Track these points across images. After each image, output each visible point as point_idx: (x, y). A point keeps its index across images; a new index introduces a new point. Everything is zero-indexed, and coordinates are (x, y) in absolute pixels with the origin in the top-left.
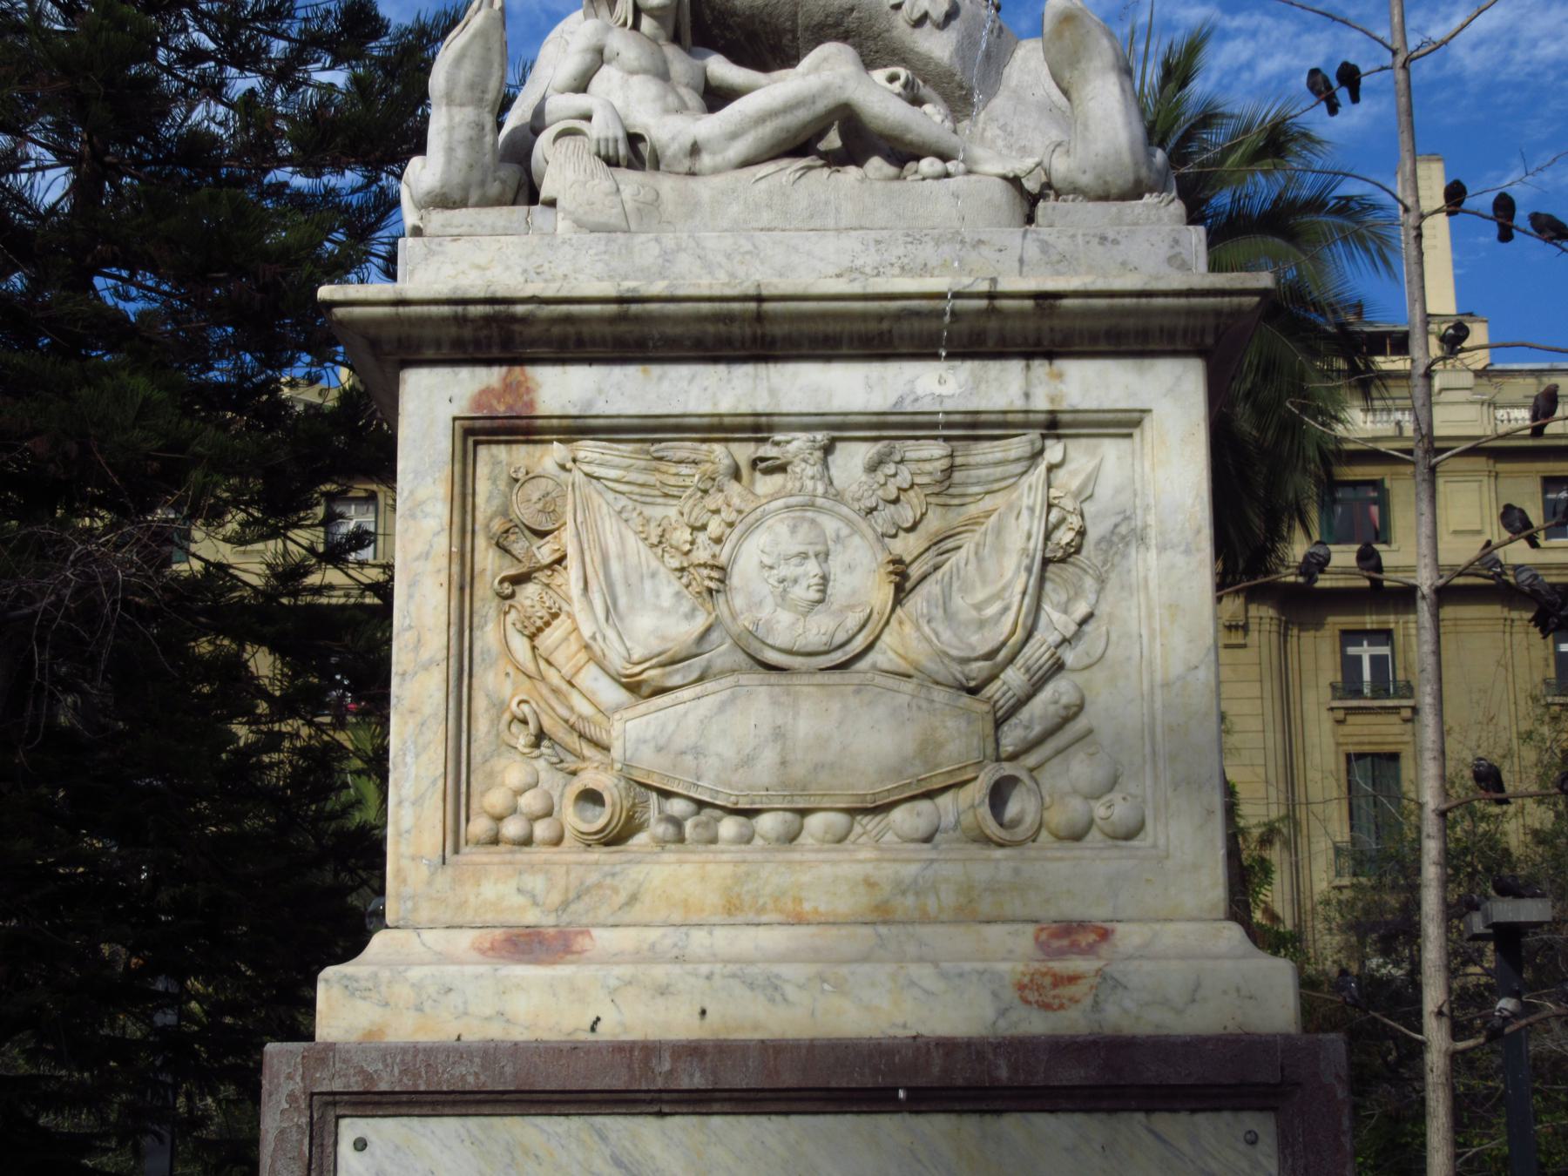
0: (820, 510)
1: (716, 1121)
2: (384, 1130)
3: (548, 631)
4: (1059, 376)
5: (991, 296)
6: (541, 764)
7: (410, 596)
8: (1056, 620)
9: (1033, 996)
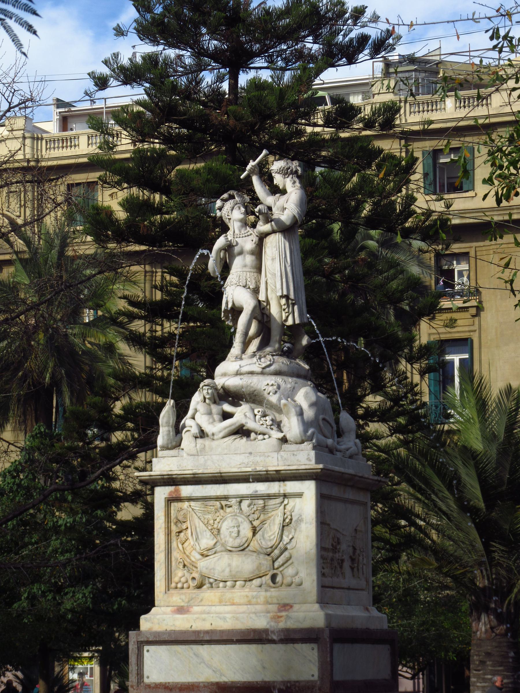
0: (238, 516)
1: (213, 646)
4: (285, 485)
5: (267, 471)
6: (185, 571)
8: (286, 539)
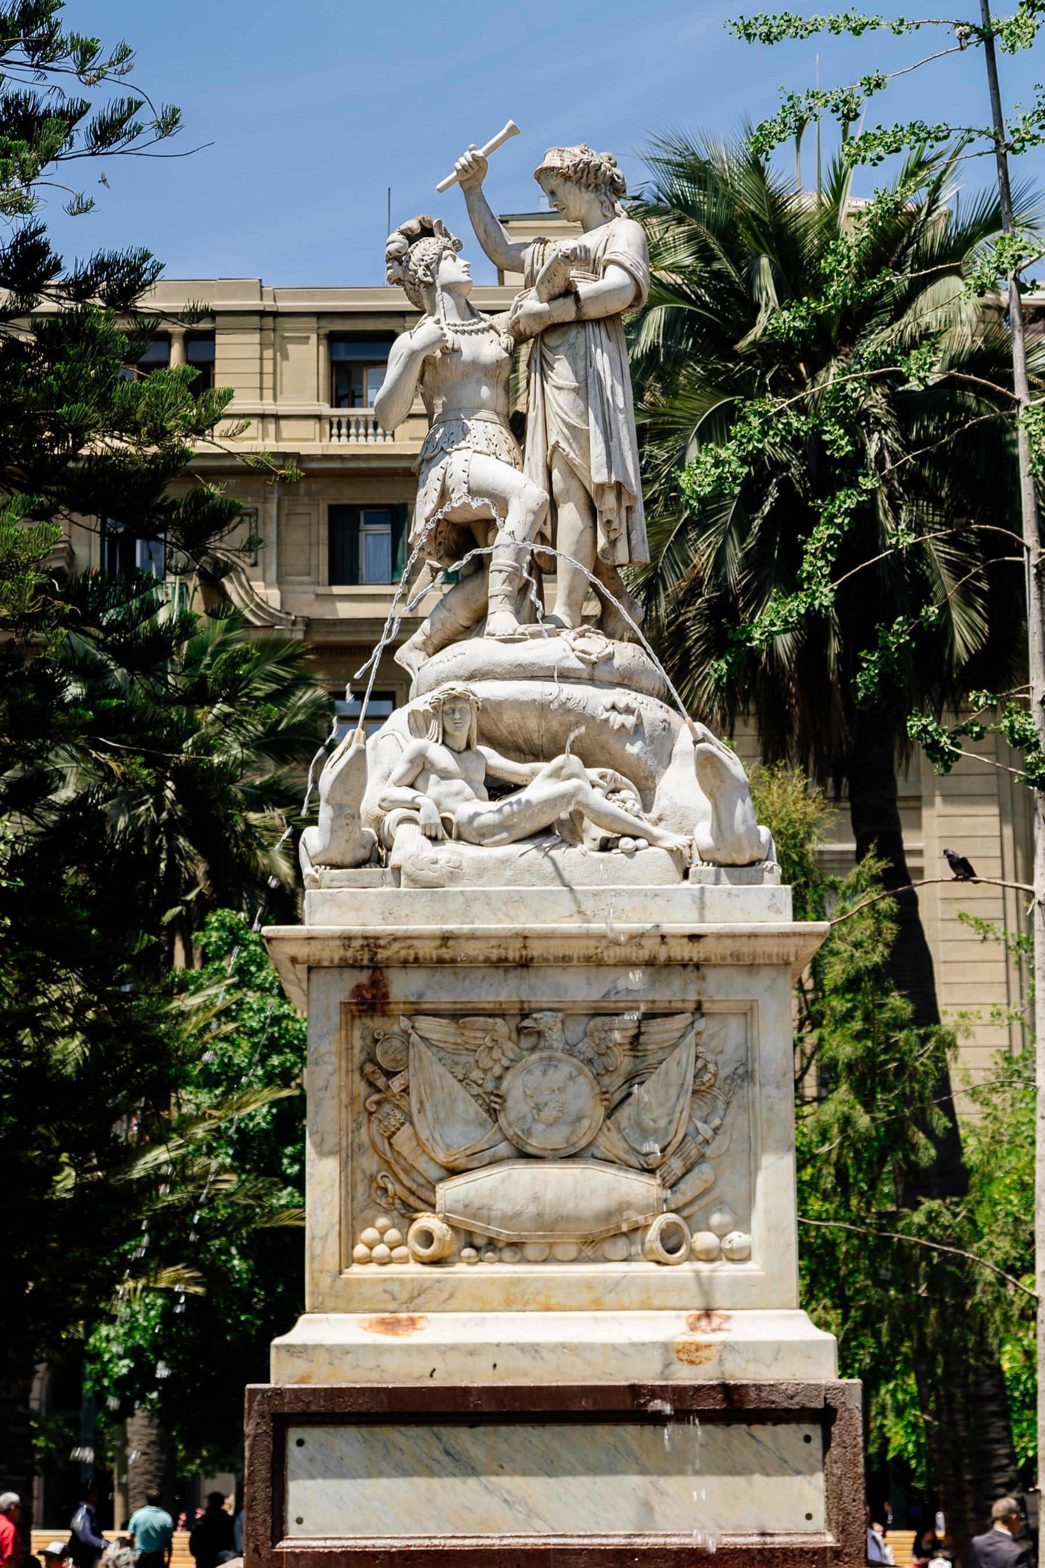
2: (314, 1435)
3: (399, 1134)
7: (317, 1113)
9: (684, 1357)
